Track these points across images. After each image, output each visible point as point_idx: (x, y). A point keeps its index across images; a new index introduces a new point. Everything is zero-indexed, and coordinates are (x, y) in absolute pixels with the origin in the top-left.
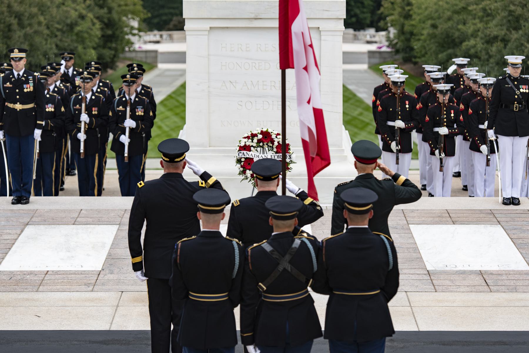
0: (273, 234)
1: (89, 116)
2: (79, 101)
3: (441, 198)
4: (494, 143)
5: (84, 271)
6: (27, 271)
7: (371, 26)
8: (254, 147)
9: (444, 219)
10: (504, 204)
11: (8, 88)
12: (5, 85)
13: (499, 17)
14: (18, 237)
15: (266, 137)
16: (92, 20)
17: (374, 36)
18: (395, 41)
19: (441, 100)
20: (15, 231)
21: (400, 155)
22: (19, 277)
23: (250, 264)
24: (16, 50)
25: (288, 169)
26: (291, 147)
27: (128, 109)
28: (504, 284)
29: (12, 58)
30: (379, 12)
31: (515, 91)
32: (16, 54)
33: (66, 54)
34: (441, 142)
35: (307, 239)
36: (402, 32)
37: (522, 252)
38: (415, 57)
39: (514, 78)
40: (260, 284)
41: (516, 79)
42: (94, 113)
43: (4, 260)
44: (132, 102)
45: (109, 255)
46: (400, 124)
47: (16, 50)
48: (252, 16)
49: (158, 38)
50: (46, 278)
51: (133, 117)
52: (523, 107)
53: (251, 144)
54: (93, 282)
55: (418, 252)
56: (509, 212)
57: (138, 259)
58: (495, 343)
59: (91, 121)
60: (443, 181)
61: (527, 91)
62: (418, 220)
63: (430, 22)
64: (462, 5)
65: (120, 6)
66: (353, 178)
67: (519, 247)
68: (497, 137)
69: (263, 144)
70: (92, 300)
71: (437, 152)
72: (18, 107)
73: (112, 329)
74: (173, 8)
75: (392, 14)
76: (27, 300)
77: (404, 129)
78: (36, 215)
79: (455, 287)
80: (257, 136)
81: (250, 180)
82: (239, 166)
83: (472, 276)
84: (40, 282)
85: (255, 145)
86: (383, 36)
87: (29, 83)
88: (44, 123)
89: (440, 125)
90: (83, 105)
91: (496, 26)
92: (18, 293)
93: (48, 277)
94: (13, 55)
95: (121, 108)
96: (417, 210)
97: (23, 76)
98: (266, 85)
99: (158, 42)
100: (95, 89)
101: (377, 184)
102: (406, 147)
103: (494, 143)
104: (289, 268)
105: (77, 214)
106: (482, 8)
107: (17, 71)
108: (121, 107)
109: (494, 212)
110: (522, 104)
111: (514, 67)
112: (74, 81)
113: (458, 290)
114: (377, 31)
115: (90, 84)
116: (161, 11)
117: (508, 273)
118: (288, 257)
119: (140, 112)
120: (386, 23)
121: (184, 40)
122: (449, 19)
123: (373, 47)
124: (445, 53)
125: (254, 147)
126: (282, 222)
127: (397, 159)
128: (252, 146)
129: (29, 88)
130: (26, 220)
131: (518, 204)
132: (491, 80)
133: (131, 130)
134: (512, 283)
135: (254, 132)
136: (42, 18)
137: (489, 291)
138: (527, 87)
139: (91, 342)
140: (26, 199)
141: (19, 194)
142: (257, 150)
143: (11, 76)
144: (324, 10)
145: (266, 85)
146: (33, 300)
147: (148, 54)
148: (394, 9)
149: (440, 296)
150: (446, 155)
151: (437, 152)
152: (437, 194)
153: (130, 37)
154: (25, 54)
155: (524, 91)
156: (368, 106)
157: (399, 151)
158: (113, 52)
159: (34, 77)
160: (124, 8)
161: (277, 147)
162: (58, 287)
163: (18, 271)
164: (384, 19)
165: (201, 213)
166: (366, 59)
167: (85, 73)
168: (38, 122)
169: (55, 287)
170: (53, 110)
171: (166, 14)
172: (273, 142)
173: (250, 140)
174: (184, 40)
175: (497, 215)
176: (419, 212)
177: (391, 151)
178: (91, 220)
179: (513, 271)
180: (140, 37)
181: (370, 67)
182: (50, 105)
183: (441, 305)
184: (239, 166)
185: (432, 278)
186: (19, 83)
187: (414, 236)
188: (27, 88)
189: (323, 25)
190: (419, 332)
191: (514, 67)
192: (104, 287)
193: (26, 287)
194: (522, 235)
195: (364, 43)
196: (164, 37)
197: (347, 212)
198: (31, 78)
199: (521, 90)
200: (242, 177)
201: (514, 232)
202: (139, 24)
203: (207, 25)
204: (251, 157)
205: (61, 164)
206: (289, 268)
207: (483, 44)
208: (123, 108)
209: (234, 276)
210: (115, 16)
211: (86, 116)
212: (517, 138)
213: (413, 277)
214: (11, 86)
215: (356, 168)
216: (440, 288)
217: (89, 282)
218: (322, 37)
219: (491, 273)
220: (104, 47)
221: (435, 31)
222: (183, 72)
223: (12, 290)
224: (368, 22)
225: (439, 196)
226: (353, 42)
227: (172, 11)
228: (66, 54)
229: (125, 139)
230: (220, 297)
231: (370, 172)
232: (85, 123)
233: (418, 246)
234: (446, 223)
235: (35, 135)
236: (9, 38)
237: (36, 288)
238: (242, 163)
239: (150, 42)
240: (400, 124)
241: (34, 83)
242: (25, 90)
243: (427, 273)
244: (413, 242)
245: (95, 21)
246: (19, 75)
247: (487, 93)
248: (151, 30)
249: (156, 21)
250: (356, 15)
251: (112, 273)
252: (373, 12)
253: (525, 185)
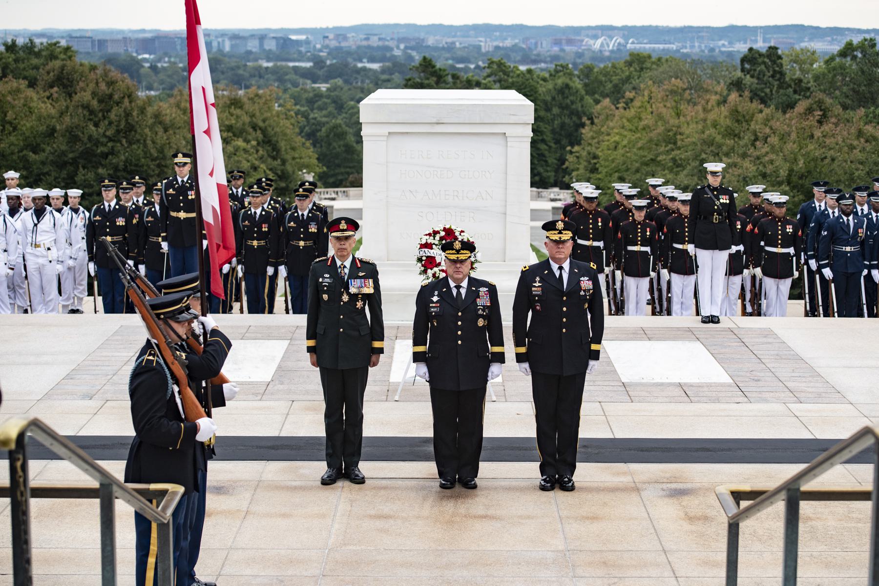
7: (555, 185)
10: (703, 322)
11: (171, 195)
13: (689, 167)
16: (265, 172)
24: (180, 155)
30: (564, 167)
37: (725, 366)
41: (715, 189)
45: (280, 368)
47: (180, 155)
48: (434, 120)
49: (333, 196)
53: (433, 242)
54: (262, 392)
58: (697, 450)
63: (617, 175)
64: (650, 156)
65: (294, 158)
72: (182, 215)
74: (350, 167)
75: (578, 169)
85: (437, 242)
91: (686, 176)
94: (176, 160)
97: (187, 182)
99: (333, 199)
100: (265, 206)
106: (672, 159)
112: (244, 201)
117: (709, 385)
119: (313, 229)
120: (571, 178)
122: (637, 171)
123: (559, 204)
131: (718, 322)
132: (688, 196)
139: (257, 447)
148: (579, 164)
149: (636, 406)
152: (630, 312)
160: (298, 160)
164: (570, 174)
171: (342, 174)
174: (360, 197)
184: (419, 265)
189: (509, 131)
190: (615, 439)
194: (723, 350)
199: (721, 201)
210: (289, 168)
212: (717, 251)
213: (607, 388)
219: (691, 386)
224: (552, 180)
227: (348, 170)
234: (641, 339)
246: (183, 181)
247: (685, 210)
250: (539, 174)
251: (282, 384)
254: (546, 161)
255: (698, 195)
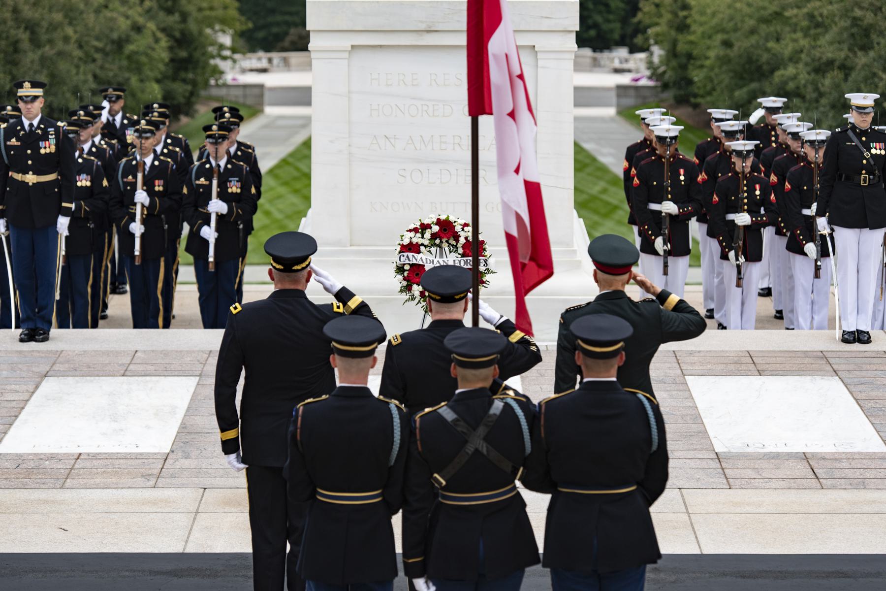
0: (457, 392)
1: (149, 195)
2: (132, 170)
3: (739, 331)
4: (828, 239)
5: (141, 454)
6: (45, 454)
7: (621, 43)
8: (426, 246)
9: (744, 367)
10: (845, 341)
11: (13, 147)
12: (8, 143)
13: (835, 29)
14: (31, 396)
15: (445, 230)
16: (154, 34)
17: (627, 61)
18: (662, 69)
19: (738, 168)
20: (24, 388)
21: (671, 260)
22: (32, 464)
23: (419, 443)
24: (27, 85)
25: (483, 282)
26: (487, 246)
27: (215, 183)
28: (843, 475)
29: (21, 97)
30: (635, 20)
31: (862, 153)
32: (27, 90)
33: (110, 90)
34: (738, 238)
35: (515, 400)
36: (672, 53)
37: (874, 421)
38: (695, 96)
39: (860, 130)
40: (436, 475)
41: (863, 133)
42: (157, 189)
43: (7, 436)
44: (222, 171)
45: (183, 427)
46: (669, 207)
47: (27, 85)
48: (423, 27)
49: (264, 64)
50: (76, 466)
51: (223, 195)
52: (877, 179)
53: (420, 241)
54: (156, 471)
55: (699, 421)
56: (853, 355)
57: (231, 434)
58: (828, 575)
59: (152, 202)
60: (743, 304)
61: (883, 152)
62: (701, 368)
63: (720, 37)
64: (773, 8)
65: (200, 10)
66: (592, 298)
67: (869, 414)
68: (832, 230)
69: (441, 242)
70: (154, 502)
71: (732, 254)
72: (31, 178)
73: (187, 551)
74: (291, 14)
75: (657, 24)
76: (46, 502)
77: (676, 216)
78: (60, 359)
79: (761, 480)
80: (431, 228)
81: (419, 302)
82: (400, 277)
83: (791, 463)
84: (67, 471)
85: (426, 242)
86: (641, 60)
87: (48, 139)
88: (73, 206)
89: (737, 210)
90: (140, 176)
91: (831, 43)
92: (31, 491)
93: (80, 464)
94: (21, 92)
95: (202, 181)
96: (699, 352)
97: (38, 127)
98: (445, 142)
99: (264, 71)
100: (159, 149)
101: (631, 308)
102: (680, 247)
103: (828, 239)
104: (484, 448)
105: (129, 359)
106: (808, 14)
107: (28, 119)
108: (202, 179)
109: (827, 355)
110: (874, 175)
111: (861, 113)
112: (124, 135)
113: (768, 485)
114: (632, 51)
115: (150, 141)
116: (270, 19)
117: (851, 457)
118: (482, 431)
120: (647, 39)
121: (307, 66)
122: (753, 31)
123: (625, 79)
124: (745, 89)
125: (426, 246)
126: (473, 372)
127: (666, 266)
128: (422, 244)
129: (48, 147)
130: (44, 368)
131: (868, 341)
132: (823, 134)
133: (220, 217)
134: (858, 474)
135: (426, 222)
136: (70, 31)
137: (819, 487)
138: (883, 145)
139: (152, 573)
140: (44, 333)
141: (31, 325)
142: (430, 251)
143: (19, 128)
144: (542, 17)
145: (445, 142)
146: (56, 502)
147: (248, 91)
148: (660, 16)
149: (736, 495)
150: (746, 260)
151: (732, 254)
152: (732, 325)
153: (218, 62)
154: (41, 90)
155: (878, 152)
156: (616, 177)
157: (668, 253)
158: (189, 88)
159: (57, 129)
160: (207, 13)
161: (464, 247)
162: (98, 481)
163: (31, 454)
164: (644, 31)
165: (336, 356)
166: (613, 98)
167: (143, 122)
168: (64, 204)
169: (92, 481)
170: (88, 184)
171: (278, 24)
172: (457, 237)
173: (419, 235)
174: (307, 66)
175: (832, 361)
176: (702, 354)
177: (656, 253)
178: (152, 368)
179: (859, 453)
180: (235, 61)
181: (620, 113)
182: (83, 176)
183: (738, 510)
184: (400, 277)
185: (724, 465)
186: (33, 139)
187: (694, 395)
188: (45, 148)
189: (540, 42)
190: (702, 556)
191: (861, 113)
192: (174, 481)
193: (43, 481)
194: (874, 394)
195: (609, 72)
196: (275, 61)
197: (581, 355)
198: (51, 130)
199: (873, 151)
200: (405, 296)
201: (861, 388)
202: (233, 41)
203: (346, 42)
204: (421, 263)
205: (102, 275)
206: (484, 448)
207: (809, 73)
208: (206, 180)
209: (392, 462)
210: (192, 26)
211: (145, 194)
212: (866, 231)
213: (692, 464)
214: (19, 143)
215: (597, 281)
216: (738, 482)
217: (150, 472)
218: (539, 61)
219: (823, 458)
220: (174, 79)
221: (728, 51)
222: (307, 121)
223: (20, 486)
224: (616, 36)
225: (736, 328)
226: (590, 71)
227: (288, 18)
228: (110, 90)
229: (209, 233)
230: (368, 497)
231: (620, 288)
232: (143, 206)
233: (701, 412)
234: (747, 373)
235: (59, 225)
236: (15, 63)
237: (61, 482)
238: (406, 274)
239: (252, 70)
240: (669, 207)
241: (57, 138)
242: (43, 151)
243: (715, 456)
244: (691, 405)
245: (160, 35)
246: (31, 125)
247: (816, 156)
248: (253, 50)
249: (261, 35)
250: (596, 26)
251: (187, 457)
252: (624, 21)
253: (879, 310)
254: (607, 5)
255: (834, 145)
